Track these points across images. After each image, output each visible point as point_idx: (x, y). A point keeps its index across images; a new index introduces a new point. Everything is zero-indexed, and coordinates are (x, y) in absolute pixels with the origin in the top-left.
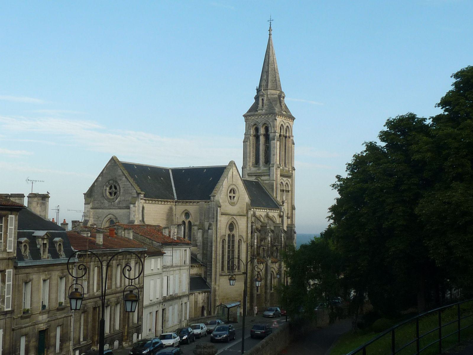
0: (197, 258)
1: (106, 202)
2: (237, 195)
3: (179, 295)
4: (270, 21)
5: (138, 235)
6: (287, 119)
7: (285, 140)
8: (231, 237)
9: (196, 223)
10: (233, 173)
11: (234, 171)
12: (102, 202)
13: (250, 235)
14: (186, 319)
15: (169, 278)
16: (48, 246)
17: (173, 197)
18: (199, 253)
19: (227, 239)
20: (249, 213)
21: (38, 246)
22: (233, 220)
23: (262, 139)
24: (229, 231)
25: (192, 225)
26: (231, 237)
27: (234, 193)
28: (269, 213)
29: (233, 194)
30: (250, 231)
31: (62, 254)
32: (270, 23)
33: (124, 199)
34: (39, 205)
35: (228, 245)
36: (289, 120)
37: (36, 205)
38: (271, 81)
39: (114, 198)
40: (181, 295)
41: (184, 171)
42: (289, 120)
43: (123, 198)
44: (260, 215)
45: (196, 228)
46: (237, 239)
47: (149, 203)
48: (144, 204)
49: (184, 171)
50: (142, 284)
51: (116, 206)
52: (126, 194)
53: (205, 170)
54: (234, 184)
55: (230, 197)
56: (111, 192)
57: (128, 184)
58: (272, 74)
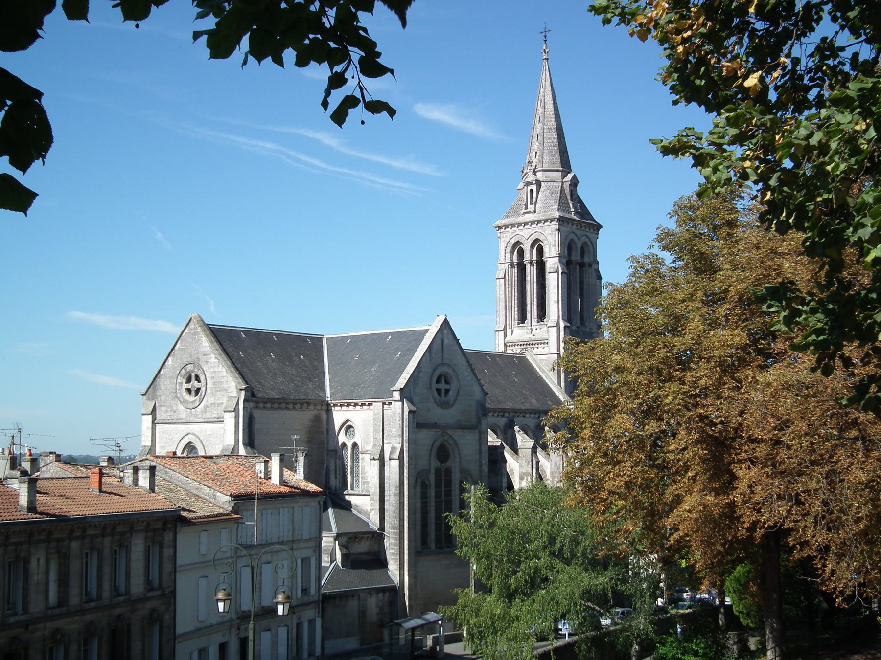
0: (369, 518)
2: (453, 386)
4: (544, 34)
5: (187, 479)
6: (583, 228)
9: (369, 447)
10: (443, 341)
11: (445, 337)
12: (175, 408)
14: (314, 655)
17: (321, 394)
18: (373, 509)
19: (432, 477)
22: (446, 437)
23: (532, 273)
27: (447, 382)
29: (446, 385)
32: (545, 37)
33: (213, 402)
35: (436, 492)
38: (549, 152)
39: (196, 400)
41: (349, 341)
42: (587, 229)
44: (526, 425)
46: (456, 476)
47: (272, 407)
49: (349, 341)
51: (200, 416)
52: (217, 391)
53: (390, 337)
55: (439, 391)
57: (220, 370)
58: (550, 139)
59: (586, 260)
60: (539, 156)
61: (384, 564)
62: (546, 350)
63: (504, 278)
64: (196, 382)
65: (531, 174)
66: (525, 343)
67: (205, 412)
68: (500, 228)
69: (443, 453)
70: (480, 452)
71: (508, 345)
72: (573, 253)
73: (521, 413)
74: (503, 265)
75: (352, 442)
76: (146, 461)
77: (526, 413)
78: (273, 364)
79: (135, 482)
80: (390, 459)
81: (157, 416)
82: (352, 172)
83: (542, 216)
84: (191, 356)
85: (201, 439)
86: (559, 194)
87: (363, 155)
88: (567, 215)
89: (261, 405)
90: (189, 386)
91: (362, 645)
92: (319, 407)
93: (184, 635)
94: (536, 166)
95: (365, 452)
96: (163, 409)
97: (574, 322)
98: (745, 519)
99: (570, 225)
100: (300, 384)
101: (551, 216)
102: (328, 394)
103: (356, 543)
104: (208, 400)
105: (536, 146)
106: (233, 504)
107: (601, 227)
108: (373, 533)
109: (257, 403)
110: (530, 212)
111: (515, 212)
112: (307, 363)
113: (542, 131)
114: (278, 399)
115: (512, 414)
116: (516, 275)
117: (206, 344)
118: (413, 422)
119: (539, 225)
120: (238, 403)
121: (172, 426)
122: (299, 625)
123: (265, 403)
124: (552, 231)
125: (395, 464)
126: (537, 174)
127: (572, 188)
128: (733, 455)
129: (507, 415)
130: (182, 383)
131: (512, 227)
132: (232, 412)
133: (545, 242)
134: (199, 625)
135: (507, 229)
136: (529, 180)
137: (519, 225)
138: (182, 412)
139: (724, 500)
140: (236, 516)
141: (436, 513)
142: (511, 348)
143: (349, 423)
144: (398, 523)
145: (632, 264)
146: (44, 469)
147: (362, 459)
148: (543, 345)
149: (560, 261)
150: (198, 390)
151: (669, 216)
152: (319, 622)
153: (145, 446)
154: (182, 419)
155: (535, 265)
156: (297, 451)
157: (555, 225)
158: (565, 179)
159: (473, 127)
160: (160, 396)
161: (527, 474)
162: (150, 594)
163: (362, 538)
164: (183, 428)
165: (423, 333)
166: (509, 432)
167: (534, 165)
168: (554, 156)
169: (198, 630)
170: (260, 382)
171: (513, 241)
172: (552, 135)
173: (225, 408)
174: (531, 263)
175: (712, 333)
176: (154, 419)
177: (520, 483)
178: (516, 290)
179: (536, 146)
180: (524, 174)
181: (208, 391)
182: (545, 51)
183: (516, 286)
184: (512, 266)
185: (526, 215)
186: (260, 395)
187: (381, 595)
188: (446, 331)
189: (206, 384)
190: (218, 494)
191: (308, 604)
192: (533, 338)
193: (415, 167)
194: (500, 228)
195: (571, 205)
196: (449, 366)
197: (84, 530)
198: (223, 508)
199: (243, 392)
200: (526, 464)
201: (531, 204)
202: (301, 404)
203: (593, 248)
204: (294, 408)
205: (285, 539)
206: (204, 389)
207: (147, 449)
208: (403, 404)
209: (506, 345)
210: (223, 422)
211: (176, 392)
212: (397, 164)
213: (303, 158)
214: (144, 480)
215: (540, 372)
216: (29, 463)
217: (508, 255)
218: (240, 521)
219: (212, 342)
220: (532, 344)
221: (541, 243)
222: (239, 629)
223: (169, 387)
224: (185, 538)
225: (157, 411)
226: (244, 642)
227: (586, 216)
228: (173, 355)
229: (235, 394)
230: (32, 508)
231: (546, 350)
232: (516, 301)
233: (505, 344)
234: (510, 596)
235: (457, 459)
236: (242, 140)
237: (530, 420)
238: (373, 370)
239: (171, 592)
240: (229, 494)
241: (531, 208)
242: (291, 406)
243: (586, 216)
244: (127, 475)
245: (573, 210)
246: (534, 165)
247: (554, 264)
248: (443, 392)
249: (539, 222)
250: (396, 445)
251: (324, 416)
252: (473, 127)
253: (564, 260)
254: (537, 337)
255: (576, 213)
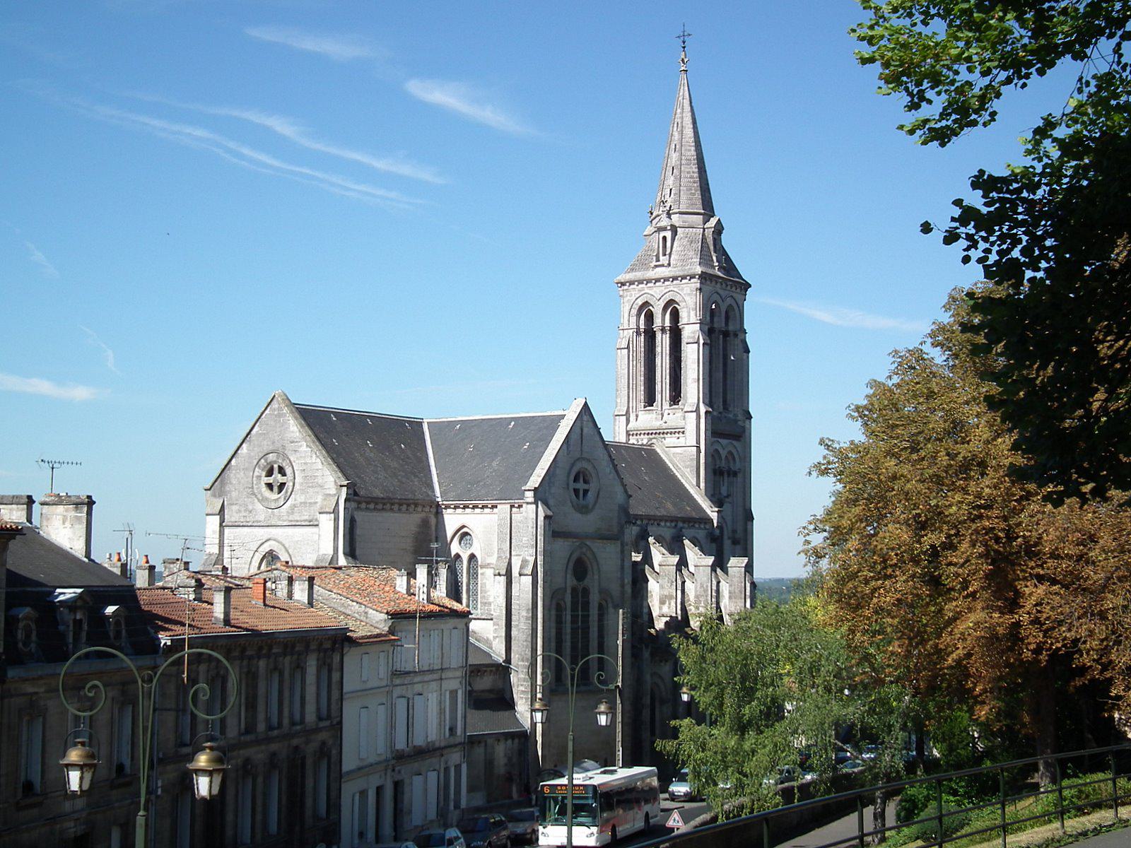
0: (491, 649)
1: (259, 506)
2: (593, 487)
3: (437, 745)
6: (729, 288)
7: (725, 341)
8: (580, 595)
9: (493, 560)
12: (250, 508)
13: (628, 589)
15: (411, 702)
16: (85, 627)
17: (430, 493)
20: (627, 531)
21: (61, 628)
22: (584, 550)
23: (663, 343)
24: (574, 579)
25: (479, 563)
26: (580, 595)
27: (586, 482)
28: (684, 530)
30: (630, 579)
31: (123, 644)
32: (684, 42)
34: (68, 524)
36: (734, 289)
37: (61, 522)
38: (687, 190)
40: (443, 744)
41: (458, 426)
42: (734, 289)
43: (301, 498)
45: (489, 572)
46: (595, 598)
47: (375, 509)
48: (355, 513)
49: (458, 426)
50: (339, 719)
51: (285, 518)
53: (513, 423)
54: (584, 459)
55: (576, 491)
56: (271, 482)
58: (688, 173)
59: (731, 328)
60: (675, 195)
61: (509, 704)
62: (682, 441)
63: (628, 348)
64: (279, 475)
65: (664, 216)
66: (654, 432)
67: (293, 513)
68: (623, 284)
69: (580, 569)
70: (622, 567)
71: (631, 433)
72: (716, 319)
73: (655, 520)
74: (626, 331)
75: (469, 552)
76: (275, 572)
77: (661, 520)
78: (372, 455)
79: (290, 595)
80: (520, 575)
81: (226, 516)
82: (317, 174)
83: (679, 271)
84: (273, 443)
85: (287, 546)
86: (700, 244)
87: (333, 150)
88: (710, 271)
89: (363, 505)
90: (270, 480)
91: (488, 802)
92: (427, 509)
93: (348, 773)
94: (671, 207)
95: (487, 566)
96: (235, 508)
97: (715, 407)
98: (1031, 639)
99: (714, 283)
100: (404, 480)
101: (691, 272)
102: (438, 493)
103: (478, 678)
104: (297, 498)
105: (670, 181)
106: (390, 623)
107: (750, 286)
108: (498, 666)
109: (359, 503)
110: (663, 266)
111: (642, 264)
112: (409, 453)
113: (679, 163)
114: (383, 498)
115: (645, 522)
116: (643, 345)
117: (294, 428)
118: (549, 530)
119: (675, 282)
120: (337, 503)
121: (246, 529)
122: (447, 769)
123: (368, 503)
124: (691, 291)
125: (527, 580)
126: (672, 216)
127: (716, 236)
128: (1019, 572)
129: (639, 522)
130: (260, 476)
131: (639, 283)
132: (330, 513)
133: (682, 304)
134: (361, 764)
135: (632, 286)
136: (662, 224)
137: (649, 281)
138: (261, 513)
139: (1009, 619)
140: (393, 637)
141: (572, 642)
142: (635, 437)
143: (465, 530)
144: (530, 654)
145: (894, 359)
146: (167, 579)
147: (482, 574)
148: (677, 435)
149: (701, 329)
150: (282, 486)
151: (944, 309)
152: (464, 767)
153: (210, 555)
154: (260, 521)
155: (668, 332)
156: (437, 562)
157: (696, 283)
158: (707, 225)
159: (490, 115)
160: (230, 492)
161: (670, 597)
162: (322, 724)
163: (486, 671)
164: (262, 533)
165: (554, 422)
166: (642, 543)
167: (668, 205)
168: (694, 194)
169: (360, 769)
170: (359, 477)
171: (640, 302)
172: (691, 168)
173: (321, 508)
174: (663, 330)
175: (1000, 440)
176: (222, 521)
177: (660, 608)
178: (642, 363)
179: (670, 181)
180: (653, 216)
181: (297, 486)
182: (683, 60)
183: (642, 359)
184: (638, 333)
185: (658, 269)
186: (362, 493)
187: (509, 742)
188: (585, 418)
189: (295, 478)
190: (371, 611)
191: (455, 746)
192: (664, 426)
193: (406, 170)
194: (623, 284)
195: (714, 258)
196: (589, 460)
197: (270, 648)
198: (378, 628)
199: (345, 489)
200: (669, 585)
201: (664, 255)
202: (408, 504)
203: (739, 310)
204: (399, 510)
205: (436, 668)
206: (291, 484)
207: (214, 558)
208: (537, 507)
209: (628, 434)
210: (317, 525)
211: (252, 488)
212: (381, 164)
213: (246, 151)
214: (300, 592)
215: (673, 469)
216: (147, 571)
217: (633, 319)
218: (399, 643)
219: (302, 427)
220: (663, 433)
221: (676, 306)
222: (393, 770)
223: (242, 481)
224: (351, 659)
225: (226, 511)
226: (398, 785)
227: (732, 272)
228: (249, 441)
229: (333, 491)
230: (227, 622)
231: (682, 441)
232: (642, 378)
233: (627, 432)
234: (742, 728)
235: (596, 577)
236: (156, 123)
237: (665, 529)
238: (494, 464)
239: (338, 724)
240: (385, 611)
241: (664, 260)
242: (396, 507)
243: (732, 272)
244: (280, 586)
245: (717, 264)
246: (668, 205)
247: (694, 332)
248: (581, 493)
249: (675, 278)
250: (527, 558)
251: (433, 521)
252: (490, 115)
253: (706, 328)
254: (670, 424)
255: (721, 268)
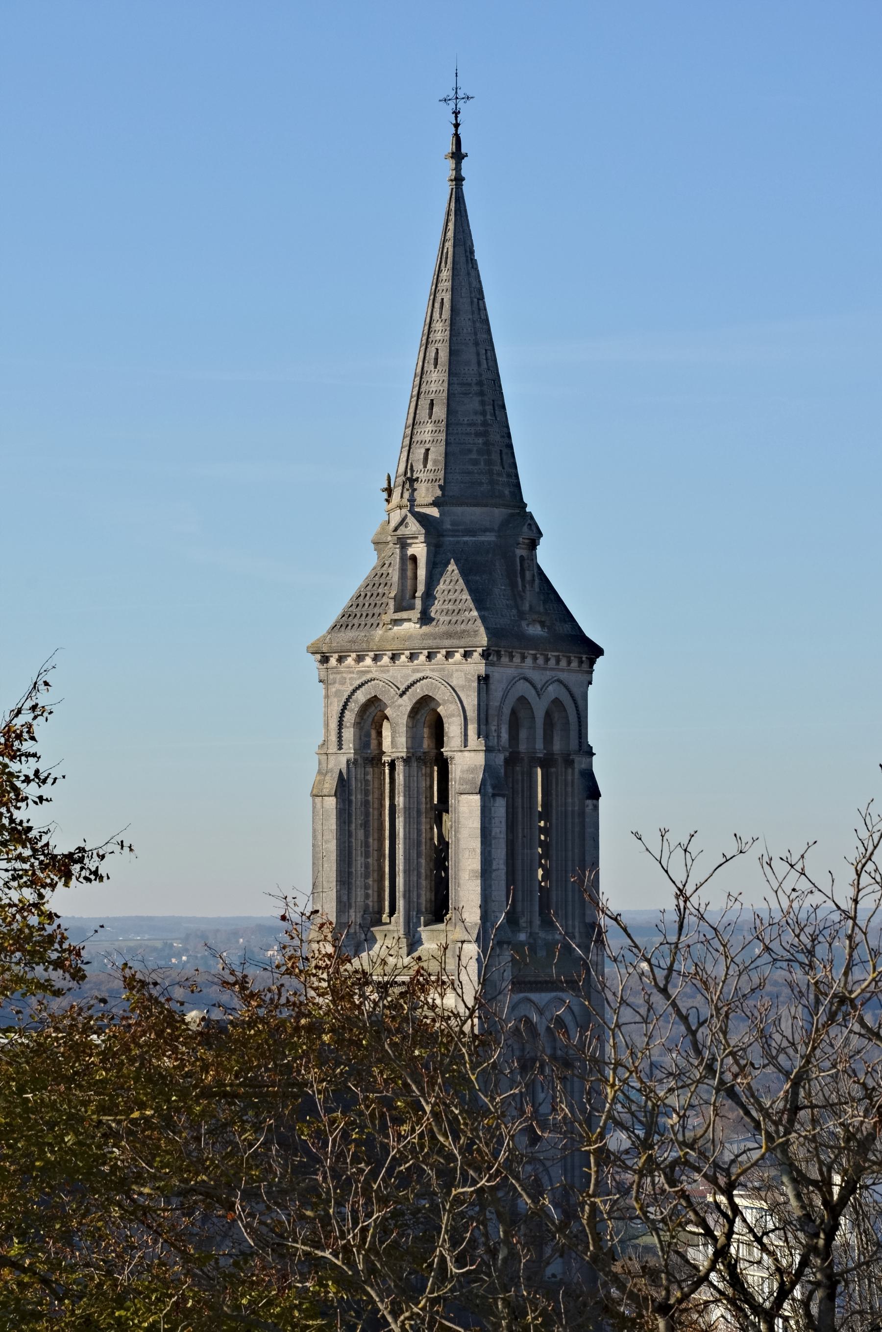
32: (456, 113)
60: (435, 462)
99: (517, 659)
124: (469, 681)
